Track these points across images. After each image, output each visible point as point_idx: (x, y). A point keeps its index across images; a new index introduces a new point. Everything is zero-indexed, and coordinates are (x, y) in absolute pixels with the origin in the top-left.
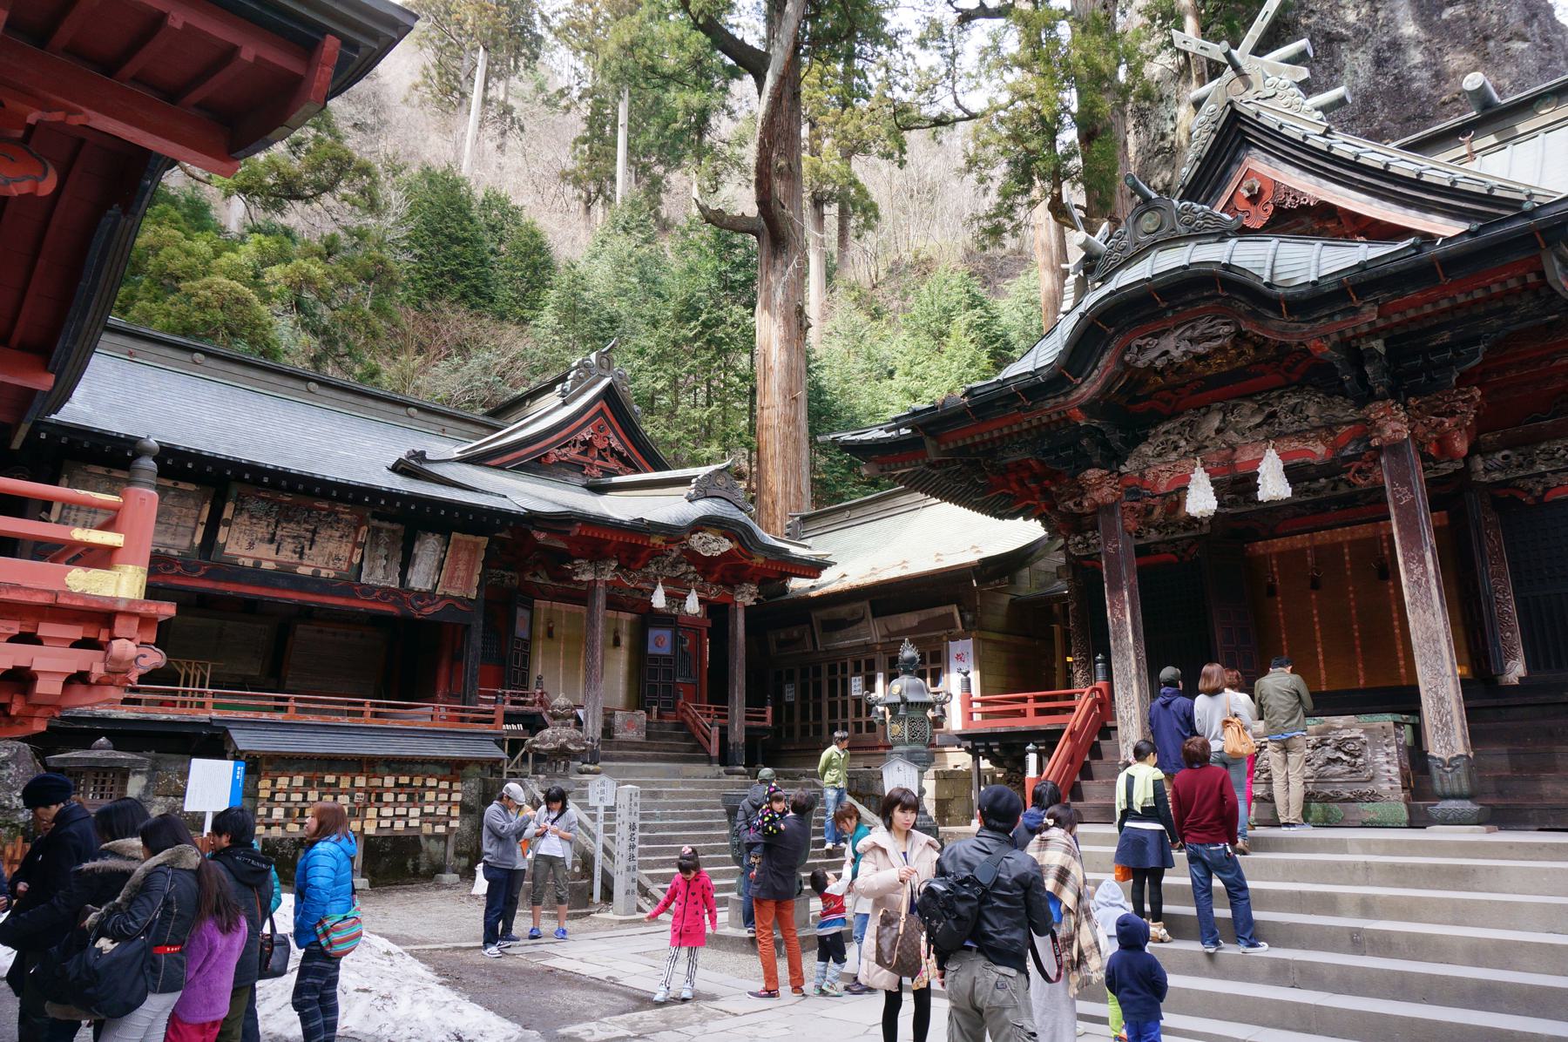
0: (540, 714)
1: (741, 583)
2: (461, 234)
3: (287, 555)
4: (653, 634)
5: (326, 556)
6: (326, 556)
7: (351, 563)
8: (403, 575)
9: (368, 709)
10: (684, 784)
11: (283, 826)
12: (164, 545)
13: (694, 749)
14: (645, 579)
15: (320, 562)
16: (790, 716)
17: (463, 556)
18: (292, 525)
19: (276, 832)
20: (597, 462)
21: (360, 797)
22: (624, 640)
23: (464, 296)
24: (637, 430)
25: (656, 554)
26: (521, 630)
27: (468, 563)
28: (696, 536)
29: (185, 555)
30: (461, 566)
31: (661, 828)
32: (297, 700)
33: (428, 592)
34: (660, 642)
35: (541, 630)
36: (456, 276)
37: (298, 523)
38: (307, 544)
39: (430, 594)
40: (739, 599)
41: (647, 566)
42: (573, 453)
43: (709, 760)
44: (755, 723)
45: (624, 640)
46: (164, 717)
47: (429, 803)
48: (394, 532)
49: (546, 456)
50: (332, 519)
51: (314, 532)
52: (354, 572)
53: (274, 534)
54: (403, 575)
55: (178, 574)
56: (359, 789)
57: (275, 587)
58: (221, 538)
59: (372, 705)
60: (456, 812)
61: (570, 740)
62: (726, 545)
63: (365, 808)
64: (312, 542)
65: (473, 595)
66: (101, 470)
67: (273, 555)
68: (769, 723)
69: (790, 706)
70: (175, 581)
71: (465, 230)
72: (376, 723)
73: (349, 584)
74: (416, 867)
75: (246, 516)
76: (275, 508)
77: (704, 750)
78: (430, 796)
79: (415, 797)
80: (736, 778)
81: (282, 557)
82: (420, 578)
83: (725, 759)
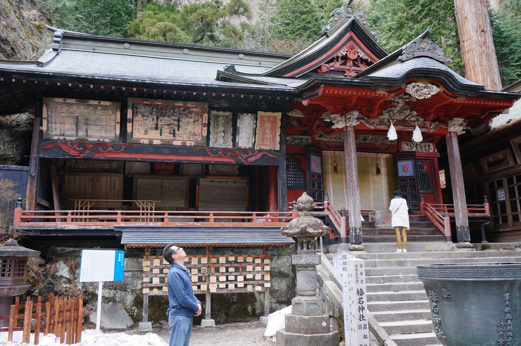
0: (328, 216)
1: (451, 119)
2: (305, 10)
3: (167, 136)
4: (401, 164)
5: (189, 133)
6: (189, 133)
7: (202, 136)
8: (234, 140)
9: (212, 217)
10: (423, 255)
11: (160, 288)
12: (102, 137)
13: (434, 233)
14: (382, 123)
15: (185, 137)
16: (504, 210)
17: (268, 125)
18: (166, 118)
19: (156, 292)
20: (353, 68)
21: (204, 269)
22: (383, 170)
23: (309, 37)
24: (374, 45)
25: (388, 105)
26: (315, 168)
27: (272, 129)
28: (410, 86)
29: (113, 141)
30: (268, 131)
31: (404, 288)
32: (169, 214)
33: (250, 149)
34: (406, 168)
35: (329, 168)
36: (305, 29)
37: (169, 116)
38: (176, 128)
39: (252, 150)
40: (451, 129)
41: (382, 114)
42: (337, 65)
43: (445, 239)
44: (477, 215)
45: (383, 170)
46: (94, 228)
47: (250, 272)
48: (227, 117)
49: (320, 68)
50: (187, 112)
51: (179, 121)
52: (205, 142)
53: (157, 124)
54: (234, 140)
55: (110, 152)
56: (204, 265)
57: (162, 154)
58: (129, 130)
59: (214, 215)
60: (267, 277)
61: (310, 226)
62: (435, 90)
63: (209, 276)
64: (179, 126)
65: (278, 148)
66: (61, 100)
67: (159, 136)
68: (488, 214)
69: (503, 204)
70: (110, 156)
71: (306, 7)
72: (218, 225)
73: (203, 148)
74: (254, 310)
75: (140, 116)
76: (155, 110)
77: (441, 233)
78: (249, 268)
79: (240, 269)
80: (465, 250)
81: (163, 137)
82: (244, 141)
83: (454, 238)
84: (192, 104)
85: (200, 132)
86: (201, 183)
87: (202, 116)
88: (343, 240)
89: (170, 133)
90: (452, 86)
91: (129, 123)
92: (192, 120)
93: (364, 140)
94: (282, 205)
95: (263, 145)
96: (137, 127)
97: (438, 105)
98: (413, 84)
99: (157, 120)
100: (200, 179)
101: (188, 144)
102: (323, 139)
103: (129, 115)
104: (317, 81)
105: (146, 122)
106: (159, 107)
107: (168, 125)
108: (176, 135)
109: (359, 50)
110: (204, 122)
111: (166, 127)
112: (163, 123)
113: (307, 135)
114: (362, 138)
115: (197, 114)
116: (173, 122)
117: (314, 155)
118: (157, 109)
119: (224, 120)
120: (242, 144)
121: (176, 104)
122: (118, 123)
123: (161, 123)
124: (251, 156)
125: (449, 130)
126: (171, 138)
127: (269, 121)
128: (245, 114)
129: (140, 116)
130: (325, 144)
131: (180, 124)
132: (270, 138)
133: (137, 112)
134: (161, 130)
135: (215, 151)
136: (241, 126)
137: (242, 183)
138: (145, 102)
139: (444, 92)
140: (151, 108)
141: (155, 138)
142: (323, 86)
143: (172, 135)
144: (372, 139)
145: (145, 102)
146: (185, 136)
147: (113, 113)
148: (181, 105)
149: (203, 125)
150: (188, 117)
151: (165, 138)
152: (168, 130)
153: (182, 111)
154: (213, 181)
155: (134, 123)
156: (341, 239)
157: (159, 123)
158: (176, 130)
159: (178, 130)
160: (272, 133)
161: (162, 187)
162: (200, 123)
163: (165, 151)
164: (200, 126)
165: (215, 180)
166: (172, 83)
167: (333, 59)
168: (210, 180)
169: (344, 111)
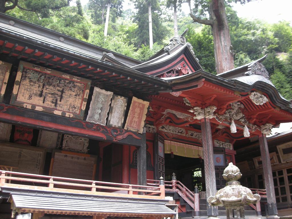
3: (49, 103)
9: (93, 186)
15: (65, 108)
18: (51, 87)
33: (119, 128)
37: (54, 86)
38: (59, 98)
51: (62, 92)
52: (82, 115)
53: (42, 92)
64: (61, 97)
67: (41, 103)
75: (28, 80)
76: (43, 77)
81: (45, 105)
84: (78, 79)
85: (79, 105)
86: (56, 156)
87: (83, 92)
88: (197, 213)
89: (53, 102)
90: (275, 99)
91: (16, 85)
92: (74, 94)
93: (191, 135)
94: (142, 181)
95: (131, 126)
96: (23, 91)
97: (260, 113)
98: (255, 93)
99: (43, 88)
100: (56, 153)
101: (67, 115)
102: (164, 130)
103: (18, 78)
104: (200, 75)
105: (32, 88)
106: (47, 76)
107: (52, 94)
108: (58, 105)
109: (188, 69)
110: (85, 97)
111: (50, 95)
112: (47, 92)
113: (153, 125)
114: (190, 134)
115: (80, 89)
116: (57, 92)
117: (160, 141)
118: (45, 77)
119: (104, 98)
120: (113, 122)
121: (63, 76)
122: (5, 83)
123: (46, 91)
124: (120, 135)
125: (262, 133)
126: (52, 107)
127: (139, 107)
128: (119, 97)
129: (28, 80)
130: (166, 135)
131: (64, 95)
132: (137, 122)
133: (26, 77)
134: (45, 97)
135: (90, 126)
136: (115, 106)
137: (92, 160)
138: (36, 69)
139: (269, 102)
140: (40, 75)
141: (37, 104)
142: (204, 80)
143: (54, 104)
144: (196, 135)
145: (36, 69)
146: (66, 107)
147: (2, 73)
148: (68, 77)
149: (83, 100)
150: (71, 90)
151: (47, 106)
152: (51, 99)
153: (67, 83)
154: (66, 156)
155: (21, 86)
156: (195, 212)
157: (45, 91)
158: (59, 100)
159: (60, 101)
160: (139, 118)
161: (20, 156)
162: (80, 97)
163: (45, 117)
164: (80, 100)
165: (68, 155)
166: (73, 53)
167: (172, 70)
168: (64, 154)
169: (204, 106)
